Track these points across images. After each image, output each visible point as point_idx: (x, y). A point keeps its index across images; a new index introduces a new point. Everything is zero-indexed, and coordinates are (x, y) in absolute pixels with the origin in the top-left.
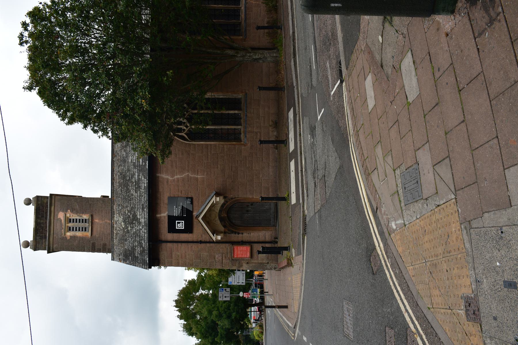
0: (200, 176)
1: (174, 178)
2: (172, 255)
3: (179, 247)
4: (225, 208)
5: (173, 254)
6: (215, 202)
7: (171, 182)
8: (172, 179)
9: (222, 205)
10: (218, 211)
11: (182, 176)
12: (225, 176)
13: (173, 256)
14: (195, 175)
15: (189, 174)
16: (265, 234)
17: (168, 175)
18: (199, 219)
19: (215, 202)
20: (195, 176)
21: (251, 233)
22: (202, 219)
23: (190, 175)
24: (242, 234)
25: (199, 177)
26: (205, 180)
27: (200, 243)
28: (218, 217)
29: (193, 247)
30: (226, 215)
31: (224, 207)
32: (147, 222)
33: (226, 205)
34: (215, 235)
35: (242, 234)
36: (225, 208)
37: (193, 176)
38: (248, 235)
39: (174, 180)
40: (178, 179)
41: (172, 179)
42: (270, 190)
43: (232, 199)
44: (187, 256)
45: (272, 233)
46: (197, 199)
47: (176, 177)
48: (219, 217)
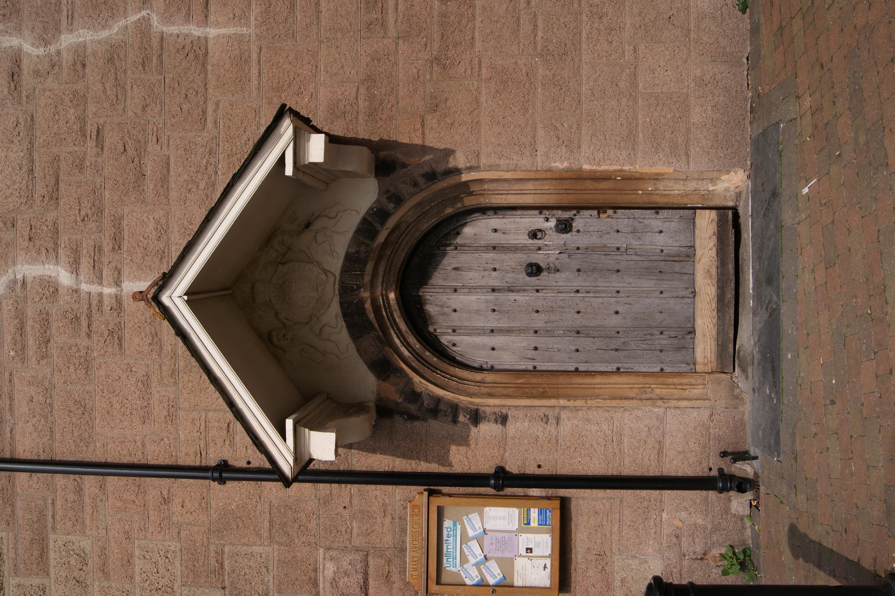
0: (217, 25)
1: (52, 49)
2: (44, 552)
3: (87, 500)
4: (381, 238)
5: (55, 541)
6: (289, 171)
7: (37, 73)
8: (41, 51)
9: (364, 220)
10: (336, 264)
11: (104, 34)
12: (384, 25)
13: (52, 555)
14: (188, 18)
15: (147, 20)
16: (661, 420)
17: (18, 29)
18: (165, 299)
19: (289, 171)
20: (184, 29)
21: (564, 415)
22: (194, 296)
23: (155, 20)
24: (503, 420)
25: (212, 32)
26: (254, 56)
27: (222, 481)
28: (335, 308)
29: (175, 507)
30: (392, 296)
31: (373, 235)
32: (541, 489)
33: (391, 223)
34: (289, 423)
35: (503, 420)
36: (381, 238)
37: (173, 29)
38: (538, 429)
39: (54, 64)
40: (80, 61)
41: (41, 51)
42: (697, 115)
43: (432, 176)
44: (138, 564)
45: (707, 413)
46: (202, 185)
47: (67, 40)
48: (342, 304)
